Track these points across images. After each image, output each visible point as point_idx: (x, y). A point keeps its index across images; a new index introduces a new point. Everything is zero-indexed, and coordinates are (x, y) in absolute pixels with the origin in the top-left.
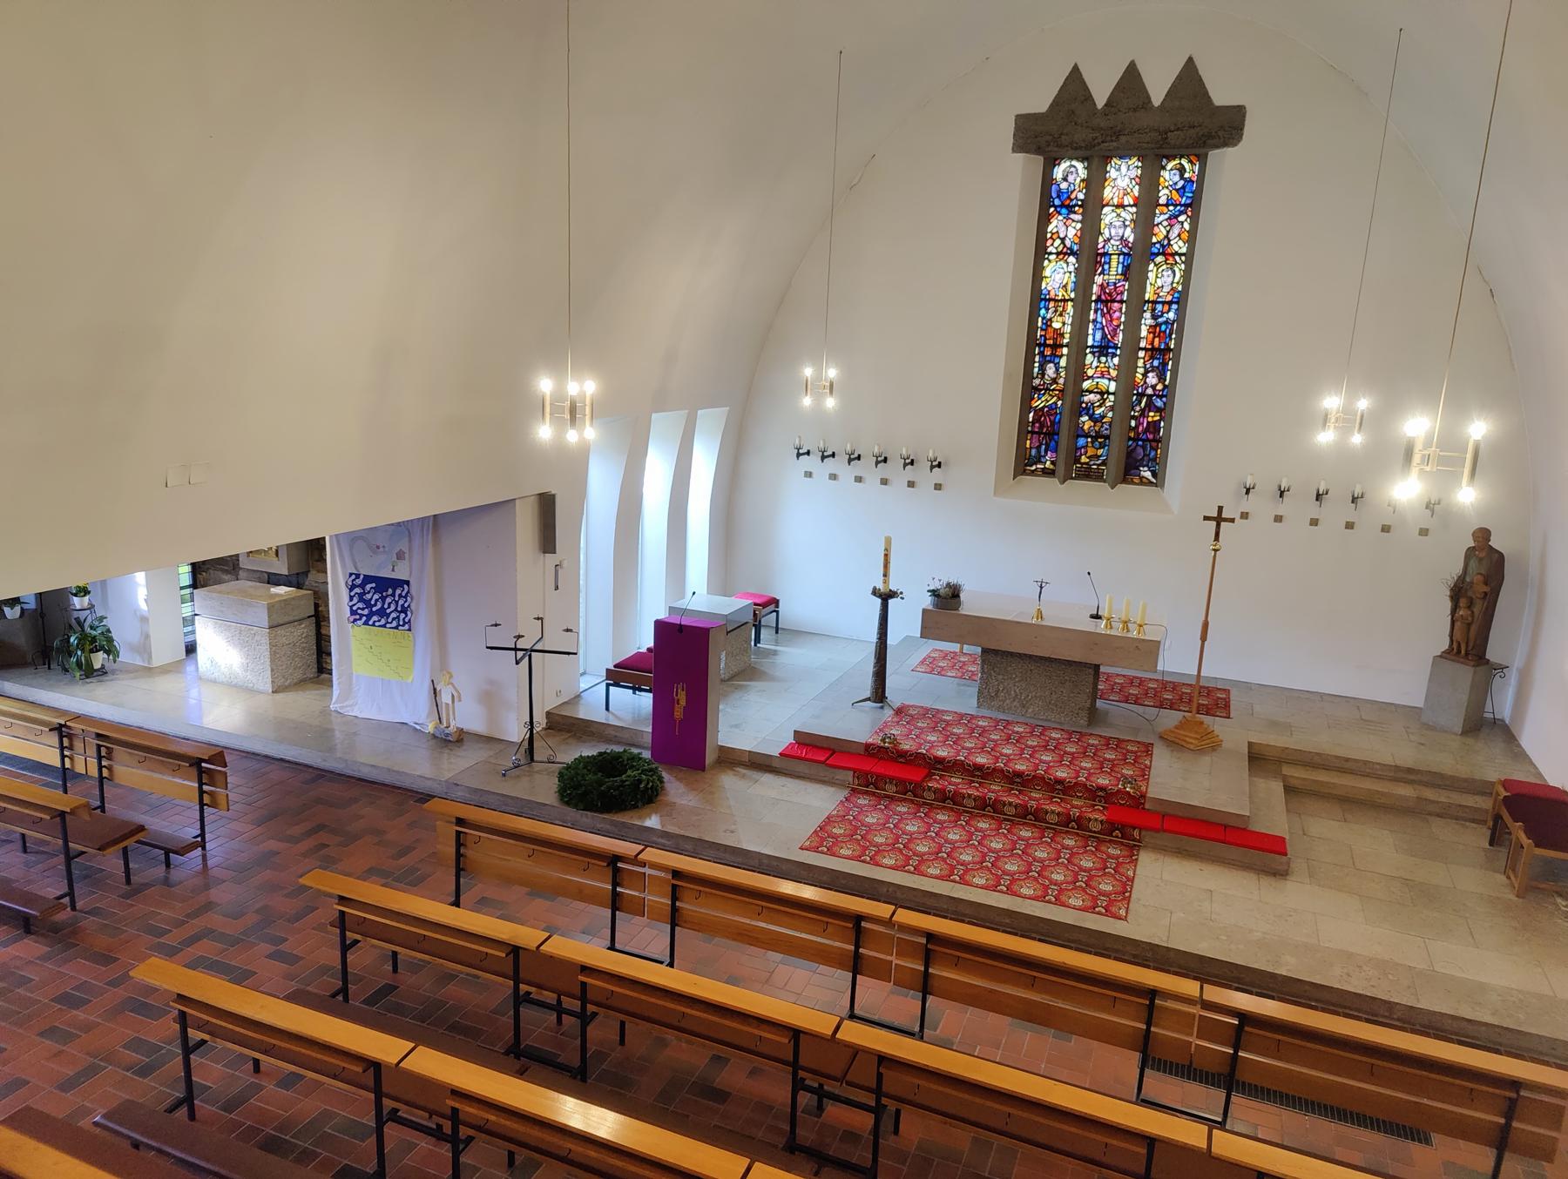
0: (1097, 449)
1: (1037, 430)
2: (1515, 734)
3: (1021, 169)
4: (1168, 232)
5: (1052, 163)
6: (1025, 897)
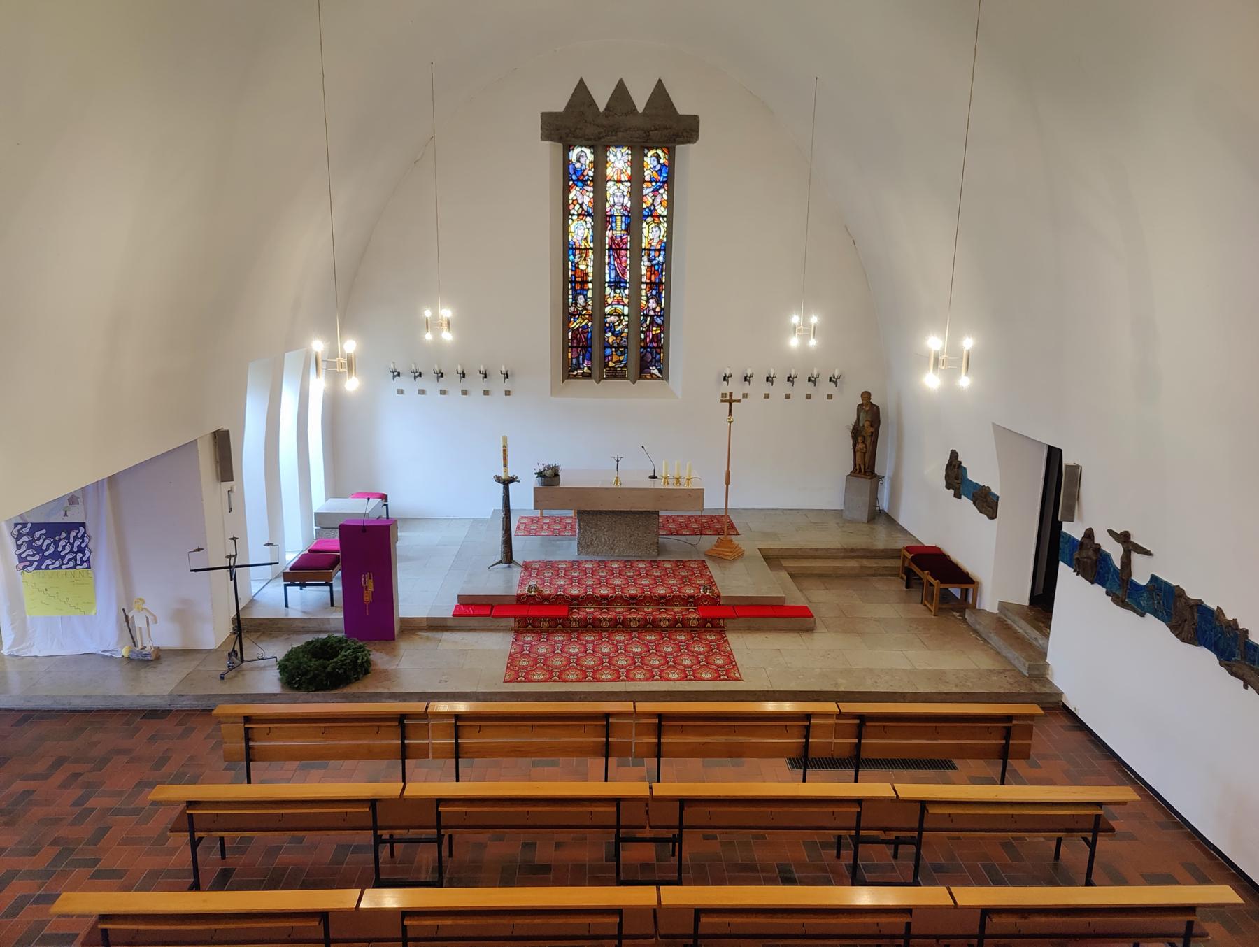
0: (620, 356)
1: (575, 345)
2: (894, 518)
3: (548, 151)
4: (653, 201)
5: (568, 148)
6: (674, 680)
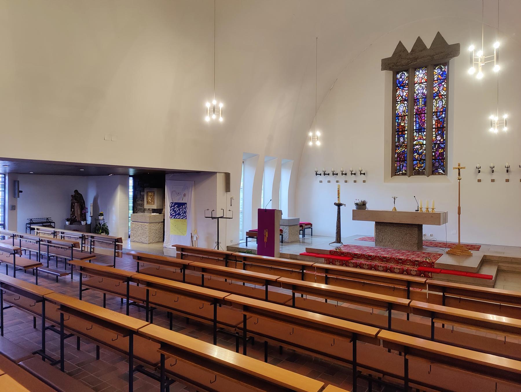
0: (421, 164)
1: (398, 160)
3: (386, 77)
4: (439, 89)
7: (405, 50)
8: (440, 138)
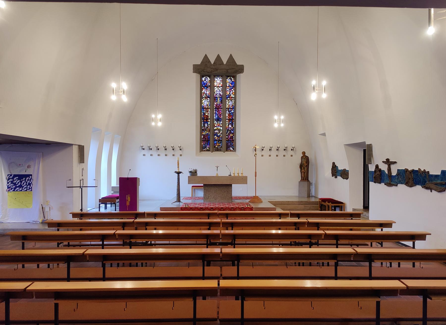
1: (204, 140)
3: (195, 77)
4: (230, 93)
7: (242, 70)
8: (231, 127)
